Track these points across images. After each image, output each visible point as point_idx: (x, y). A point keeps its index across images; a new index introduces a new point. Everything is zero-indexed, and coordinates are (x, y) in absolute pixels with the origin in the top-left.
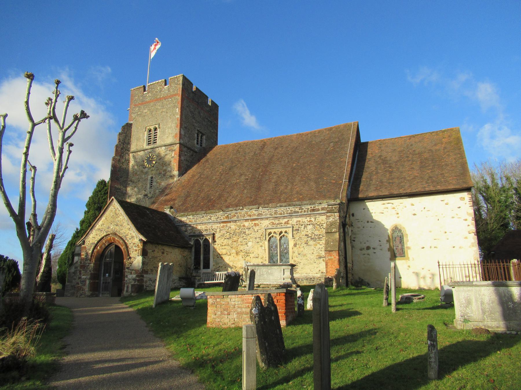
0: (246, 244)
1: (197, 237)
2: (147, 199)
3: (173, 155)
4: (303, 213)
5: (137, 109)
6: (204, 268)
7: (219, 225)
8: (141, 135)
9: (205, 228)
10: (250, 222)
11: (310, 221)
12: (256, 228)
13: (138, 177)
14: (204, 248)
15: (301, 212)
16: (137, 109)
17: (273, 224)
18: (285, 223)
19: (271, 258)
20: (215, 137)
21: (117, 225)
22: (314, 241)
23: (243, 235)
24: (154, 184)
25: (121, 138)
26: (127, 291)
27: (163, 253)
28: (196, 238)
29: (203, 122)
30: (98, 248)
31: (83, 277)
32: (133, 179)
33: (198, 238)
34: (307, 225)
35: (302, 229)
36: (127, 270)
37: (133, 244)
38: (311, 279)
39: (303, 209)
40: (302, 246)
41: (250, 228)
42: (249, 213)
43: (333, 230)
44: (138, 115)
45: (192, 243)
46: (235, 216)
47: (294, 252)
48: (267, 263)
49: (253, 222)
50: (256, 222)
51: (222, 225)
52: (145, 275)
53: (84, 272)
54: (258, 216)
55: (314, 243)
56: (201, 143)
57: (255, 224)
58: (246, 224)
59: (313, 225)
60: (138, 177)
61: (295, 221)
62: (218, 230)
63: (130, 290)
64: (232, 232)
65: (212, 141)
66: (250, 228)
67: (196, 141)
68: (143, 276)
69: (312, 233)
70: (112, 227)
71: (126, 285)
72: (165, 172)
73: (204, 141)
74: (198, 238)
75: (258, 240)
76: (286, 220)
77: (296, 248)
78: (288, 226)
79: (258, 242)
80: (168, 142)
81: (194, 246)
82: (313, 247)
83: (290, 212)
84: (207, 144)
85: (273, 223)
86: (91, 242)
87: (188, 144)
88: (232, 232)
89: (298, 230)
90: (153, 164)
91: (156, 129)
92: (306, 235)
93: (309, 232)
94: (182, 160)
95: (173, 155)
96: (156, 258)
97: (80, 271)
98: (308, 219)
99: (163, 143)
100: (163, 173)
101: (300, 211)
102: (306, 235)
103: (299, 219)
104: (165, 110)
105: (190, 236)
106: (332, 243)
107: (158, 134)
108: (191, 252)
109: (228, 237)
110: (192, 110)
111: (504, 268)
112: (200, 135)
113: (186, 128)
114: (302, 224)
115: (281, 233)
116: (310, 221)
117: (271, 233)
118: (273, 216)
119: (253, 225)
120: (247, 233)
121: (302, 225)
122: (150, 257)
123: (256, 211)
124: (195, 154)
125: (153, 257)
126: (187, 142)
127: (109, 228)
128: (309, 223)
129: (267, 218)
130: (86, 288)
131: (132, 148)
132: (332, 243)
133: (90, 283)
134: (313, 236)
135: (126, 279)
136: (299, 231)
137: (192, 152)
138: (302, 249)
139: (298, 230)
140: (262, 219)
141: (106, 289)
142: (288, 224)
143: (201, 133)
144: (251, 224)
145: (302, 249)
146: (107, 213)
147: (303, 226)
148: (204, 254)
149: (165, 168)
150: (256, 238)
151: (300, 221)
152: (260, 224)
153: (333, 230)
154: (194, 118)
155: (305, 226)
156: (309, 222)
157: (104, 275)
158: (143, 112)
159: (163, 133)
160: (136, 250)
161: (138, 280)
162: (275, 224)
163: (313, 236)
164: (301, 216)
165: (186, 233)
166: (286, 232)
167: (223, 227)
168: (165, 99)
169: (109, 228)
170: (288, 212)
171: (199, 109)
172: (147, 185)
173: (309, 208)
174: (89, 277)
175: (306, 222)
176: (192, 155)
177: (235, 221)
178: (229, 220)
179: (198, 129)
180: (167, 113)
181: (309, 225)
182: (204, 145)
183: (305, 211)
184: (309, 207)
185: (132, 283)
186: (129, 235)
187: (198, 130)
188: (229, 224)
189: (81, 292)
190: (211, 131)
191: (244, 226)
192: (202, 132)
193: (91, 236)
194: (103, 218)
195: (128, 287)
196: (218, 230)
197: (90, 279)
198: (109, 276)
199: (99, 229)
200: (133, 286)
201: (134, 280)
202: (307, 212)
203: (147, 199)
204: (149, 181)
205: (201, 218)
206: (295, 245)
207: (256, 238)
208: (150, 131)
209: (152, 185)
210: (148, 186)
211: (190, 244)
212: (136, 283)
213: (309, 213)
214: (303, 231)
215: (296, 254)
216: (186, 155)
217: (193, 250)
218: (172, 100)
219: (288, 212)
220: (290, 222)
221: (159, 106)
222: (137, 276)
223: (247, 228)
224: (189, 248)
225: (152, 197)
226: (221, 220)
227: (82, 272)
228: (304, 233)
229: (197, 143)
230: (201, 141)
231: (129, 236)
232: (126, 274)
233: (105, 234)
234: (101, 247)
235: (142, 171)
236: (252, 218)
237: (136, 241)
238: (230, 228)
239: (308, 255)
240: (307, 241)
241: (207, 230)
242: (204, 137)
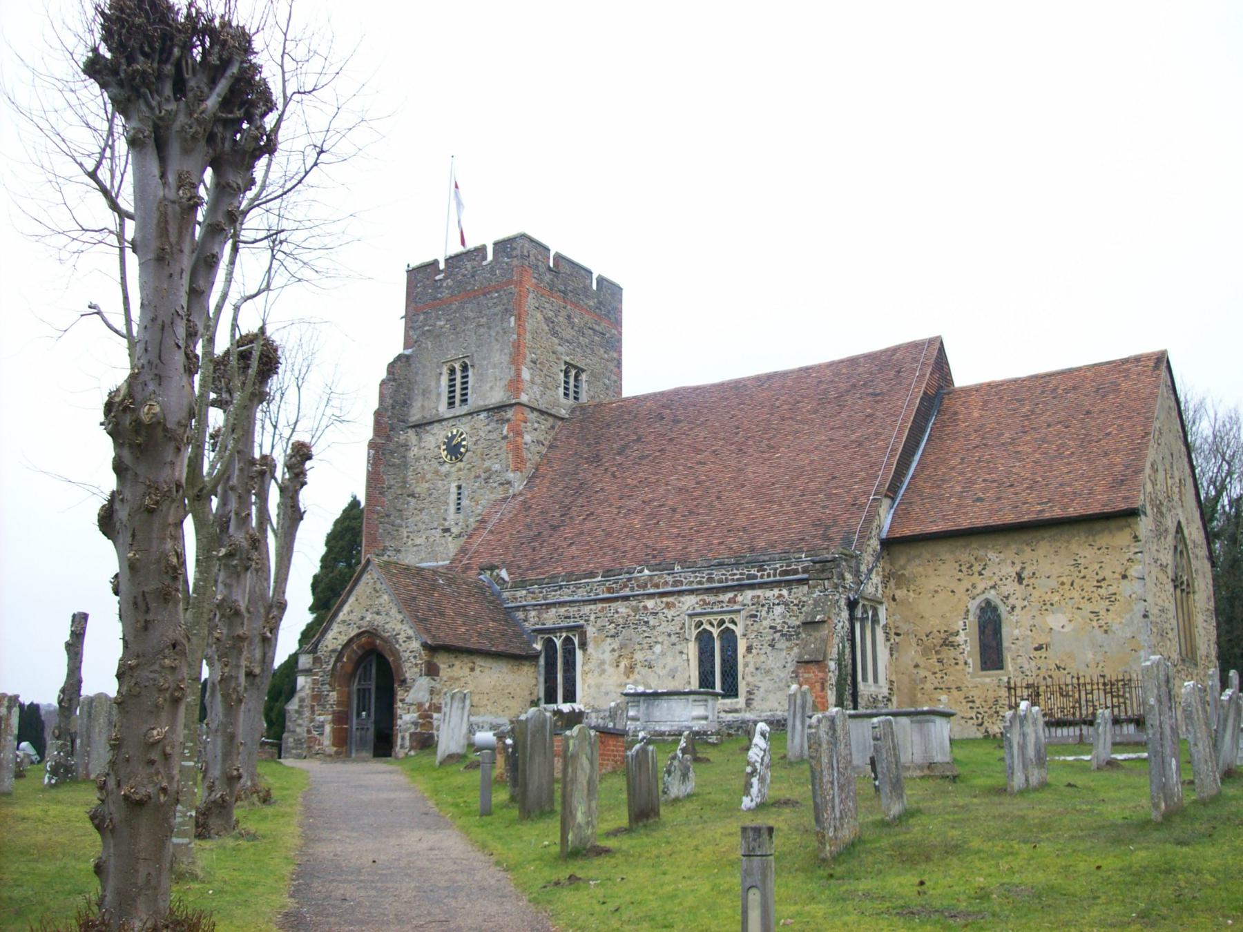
0: (651, 648)
1: (549, 633)
2: (450, 539)
3: (505, 432)
4: (766, 579)
5: (422, 317)
6: (565, 701)
7: (593, 607)
8: (433, 384)
9: (566, 614)
10: (658, 600)
11: (781, 596)
12: (670, 613)
13: (427, 485)
14: (565, 657)
15: (762, 577)
16: (422, 317)
17: (705, 603)
18: (729, 602)
19: (706, 679)
20: (615, 370)
21: (378, 613)
22: (787, 640)
23: (644, 628)
24: (465, 502)
25: (385, 392)
26: (402, 747)
27: (472, 669)
28: (546, 636)
29: (581, 338)
30: (345, 660)
31: (318, 718)
32: (418, 490)
33: (552, 636)
34: (774, 604)
35: (764, 613)
36: (400, 704)
37: (411, 652)
38: (778, 721)
39: (765, 570)
40: (763, 651)
41: (657, 613)
42: (656, 579)
43: (818, 617)
44: (424, 333)
45: (538, 646)
46: (626, 586)
47: (746, 665)
48: (695, 685)
49: (664, 600)
50: (670, 599)
51: (600, 606)
52: (435, 715)
53: (320, 708)
54: (673, 586)
55: (788, 644)
56: (576, 392)
57: (667, 604)
58: (650, 604)
59: (786, 604)
60: (427, 485)
61: (749, 597)
62: (592, 617)
63: (407, 743)
64: (621, 621)
65: (607, 382)
66: (657, 613)
67: (561, 391)
68: (431, 717)
69: (784, 622)
70: (369, 617)
71: (399, 735)
72: (487, 474)
73: (584, 386)
74: (552, 636)
75: (674, 639)
76: (731, 595)
77: (751, 656)
78: (736, 607)
79: (674, 644)
80: (493, 401)
81: (543, 655)
82: (784, 653)
83: (738, 576)
84: (592, 393)
85: (704, 600)
86: (330, 648)
87: (541, 401)
88: (621, 621)
89: (756, 616)
90: (461, 453)
91: (465, 368)
92: (771, 627)
93: (778, 621)
94: (526, 444)
95: (505, 432)
96: (458, 679)
97: (313, 707)
98: (776, 592)
99: (481, 403)
100: (483, 476)
101: (759, 574)
102: (771, 627)
103: (758, 592)
104: (483, 320)
105: (534, 631)
106: (813, 646)
107: (471, 380)
108: (537, 665)
109: (613, 632)
110: (551, 314)
111: (876, 680)
112: (573, 372)
113: (534, 362)
114: (764, 602)
115: (722, 622)
116: (781, 596)
117: (702, 624)
118: (706, 586)
119: (663, 605)
120: (651, 623)
121: (763, 606)
122: (445, 679)
123: (669, 574)
124: (560, 423)
125: (451, 678)
126: (538, 397)
127: (362, 618)
128: (777, 602)
129: (691, 592)
130: (327, 741)
131: (414, 415)
132: (813, 646)
133: (334, 731)
134: (786, 629)
135: (399, 722)
136: (757, 619)
137: (551, 420)
138: (763, 658)
139: (756, 616)
140: (681, 593)
141: (362, 744)
142: (735, 602)
143: (575, 367)
144: (659, 604)
145: (763, 658)
146: (360, 588)
147: (766, 608)
148: (565, 671)
149: (487, 464)
150: (669, 635)
151: (759, 597)
152: (677, 605)
153: (818, 617)
154: (555, 334)
155: (769, 608)
156: (778, 597)
157: (359, 715)
158: (434, 325)
159: (481, 378)
160: (416, 665)
161: (422, 725)
162: (709, 603)
163: (786, 629)
164: (761, 586)
165: (526, 624)
166: (733, 622)
167: (602, 610)
168: (484, 295)
169: (362, 618)
170: (735, 577)
171: (569, 307)
172: (448, 504)
173: (777, 569)
174: (330, 717)
175: (772, 598)
176: (553, 427)
177: (626, 598)
178: (615, 595)
179: (568, 359)
180: (489, 328)
181: (778, 604)
182: (584, 398)
183: (769, 575)
184: (778, 566)
185: (412, 731)
186: (402, 633)
187: (566, 363)
188: (614, 605)
189: (317, 748)
190: (602, 358)
191: (645, 608)
192: (579, 365)
193: (330, 635)
194: (352, 599)
195: (403, 738)
196: (592, 617)
197: (334, 721)
198: (368, 715)
199: (344, 622)
200: (411, 735)
201: (415, 724)
202: (775, 575)
203: (450, 539)
204: (453, 497)
205: (556, 591)
206: (749, 649)
207: (669, 635)
208: (452, 371)
209: (459, 504)
210: (452, 508)
211: (535, 649)
212: (419, 730)
213: (778, 578)
214: (765, 618)
215: (751, 668)
216: (535, 429)
217: (542, 661)
218: (500, 296)
219: (735, 577)
220: (740, 598)
221: (472, 311)
222: (420, 717)
223: (651, 613)
224: (522, 658)
225: (459, 536)
226: (597, 594)
227: (316, 708)
228: (766, 623)
229: (566, 395)
230: (576, 386)
231: (401, 638)
232: (399, 712)
233: (356, 631)
234: (349, 658)
235: (436, 472)
236: (661, 590)
237: (415, 645)
238: (617, 612)
239: (776, 672)
240: (773, 640)
241: (569, 617)
242: (584, 377)
